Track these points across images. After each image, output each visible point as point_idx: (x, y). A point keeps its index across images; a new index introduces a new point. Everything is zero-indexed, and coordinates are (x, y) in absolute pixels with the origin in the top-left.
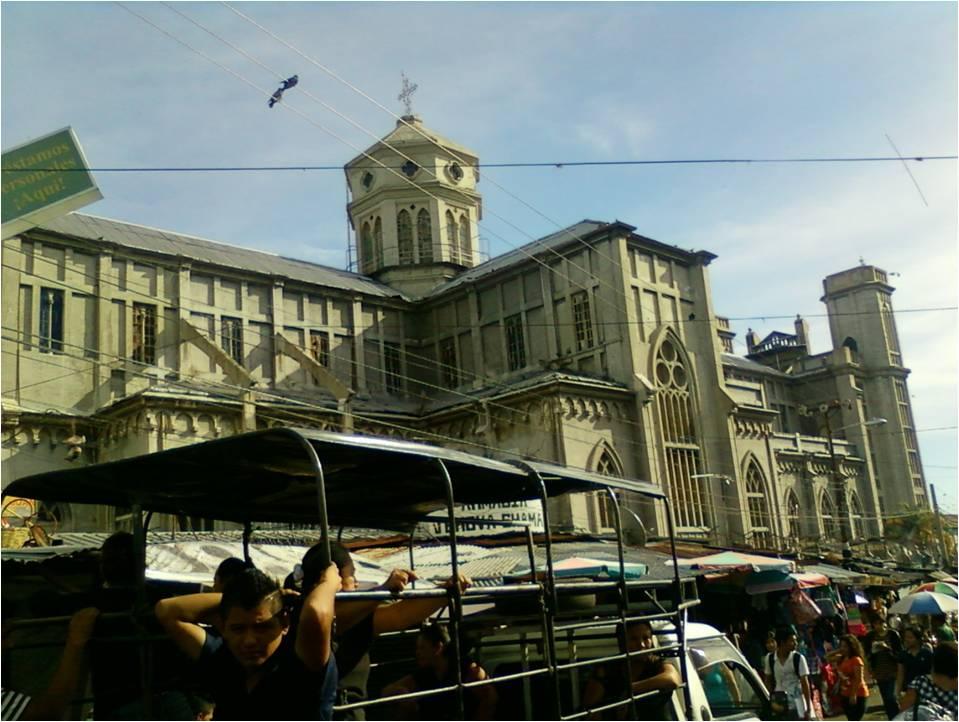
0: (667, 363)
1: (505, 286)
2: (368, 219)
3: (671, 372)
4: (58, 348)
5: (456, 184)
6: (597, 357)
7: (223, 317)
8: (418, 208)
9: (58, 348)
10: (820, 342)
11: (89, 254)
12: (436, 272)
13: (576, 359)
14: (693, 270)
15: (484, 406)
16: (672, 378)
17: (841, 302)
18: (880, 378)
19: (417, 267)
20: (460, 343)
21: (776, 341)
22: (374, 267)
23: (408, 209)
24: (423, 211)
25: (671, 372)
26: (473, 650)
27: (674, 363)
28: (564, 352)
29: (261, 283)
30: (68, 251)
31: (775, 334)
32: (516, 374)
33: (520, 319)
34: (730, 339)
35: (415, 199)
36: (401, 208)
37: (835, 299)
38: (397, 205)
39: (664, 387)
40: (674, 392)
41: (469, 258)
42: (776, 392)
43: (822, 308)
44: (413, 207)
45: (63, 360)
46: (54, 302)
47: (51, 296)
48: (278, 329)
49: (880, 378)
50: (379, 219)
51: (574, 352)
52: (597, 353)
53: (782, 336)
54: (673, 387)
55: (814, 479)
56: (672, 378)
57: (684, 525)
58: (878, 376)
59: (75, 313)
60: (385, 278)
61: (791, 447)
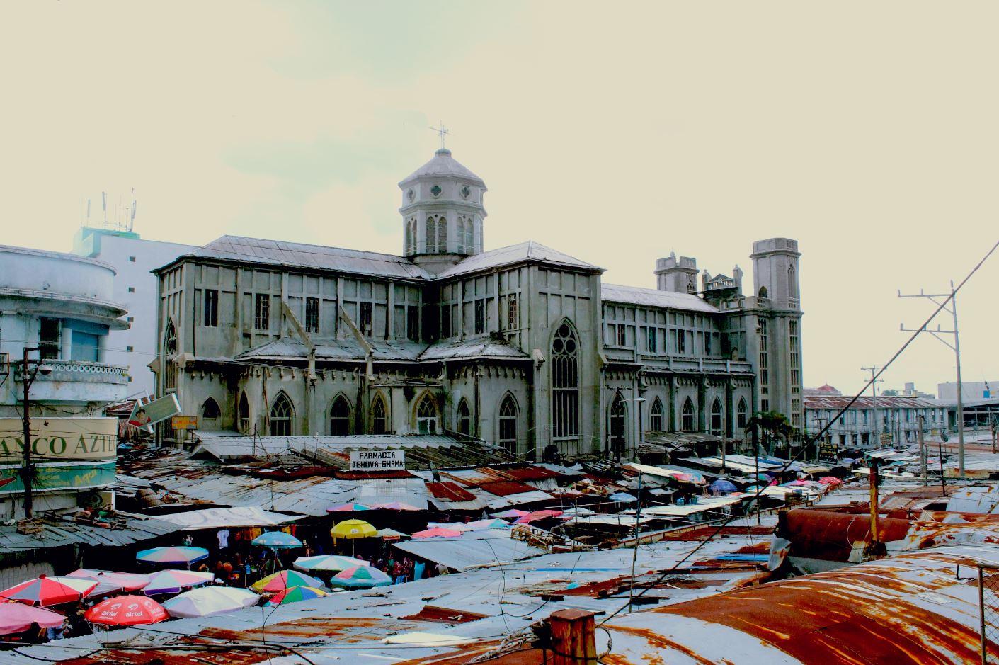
0: (562, 339)
1: (477, 280)
2: (410, 220)
3: (564, 344)
4: (215, 324)
5: (465, 200)
6: (518, 335)
7: (307, 298)
8: (439, 217)
9: (215, 324)
10: (748, 289)
11: (234, 269)
12: (448, 258)
13: (508, 334)
14: (591, 277)
15: (444, 364)
16: (565, 347)
17: (762, 261)
18: (778, 318)
19: (436, 255)
20: (452, 310)
21: (720, 280)
22: (412, 254)
23: (434, 217)
24: (442, 218)
25: (564, 344)
26: (227, 565)
27: (567, 339)
28: (503, 329)
29: (332, 275)
30: (220, 268)
31: (720, 276)
32: (478, 336)
33: (482, 303)
34: (694, 274)
35: (438, 211)
36: (429, 216)
37: (758, 258)
38: (426, 214)
39: (557, 354)
40: (565, 356)
41: (472, 249)
42: (704, 323)
43: (751, 262)
44: (436, 216)
45: (217, 329)
46: (212, 298)
47: (211, 293)
48: (340, 303)
49: (778, 318)
50: (416, 221)
51: (507, 330)
52: (518, 333)
53: (724, 278)
54: (564, 353)
55: (706, 390)
56: (565, 347)
57: (560, 435)
58: (777, 316)
59: (224, 303)
60: (417, 260)
61: (696, 367)
